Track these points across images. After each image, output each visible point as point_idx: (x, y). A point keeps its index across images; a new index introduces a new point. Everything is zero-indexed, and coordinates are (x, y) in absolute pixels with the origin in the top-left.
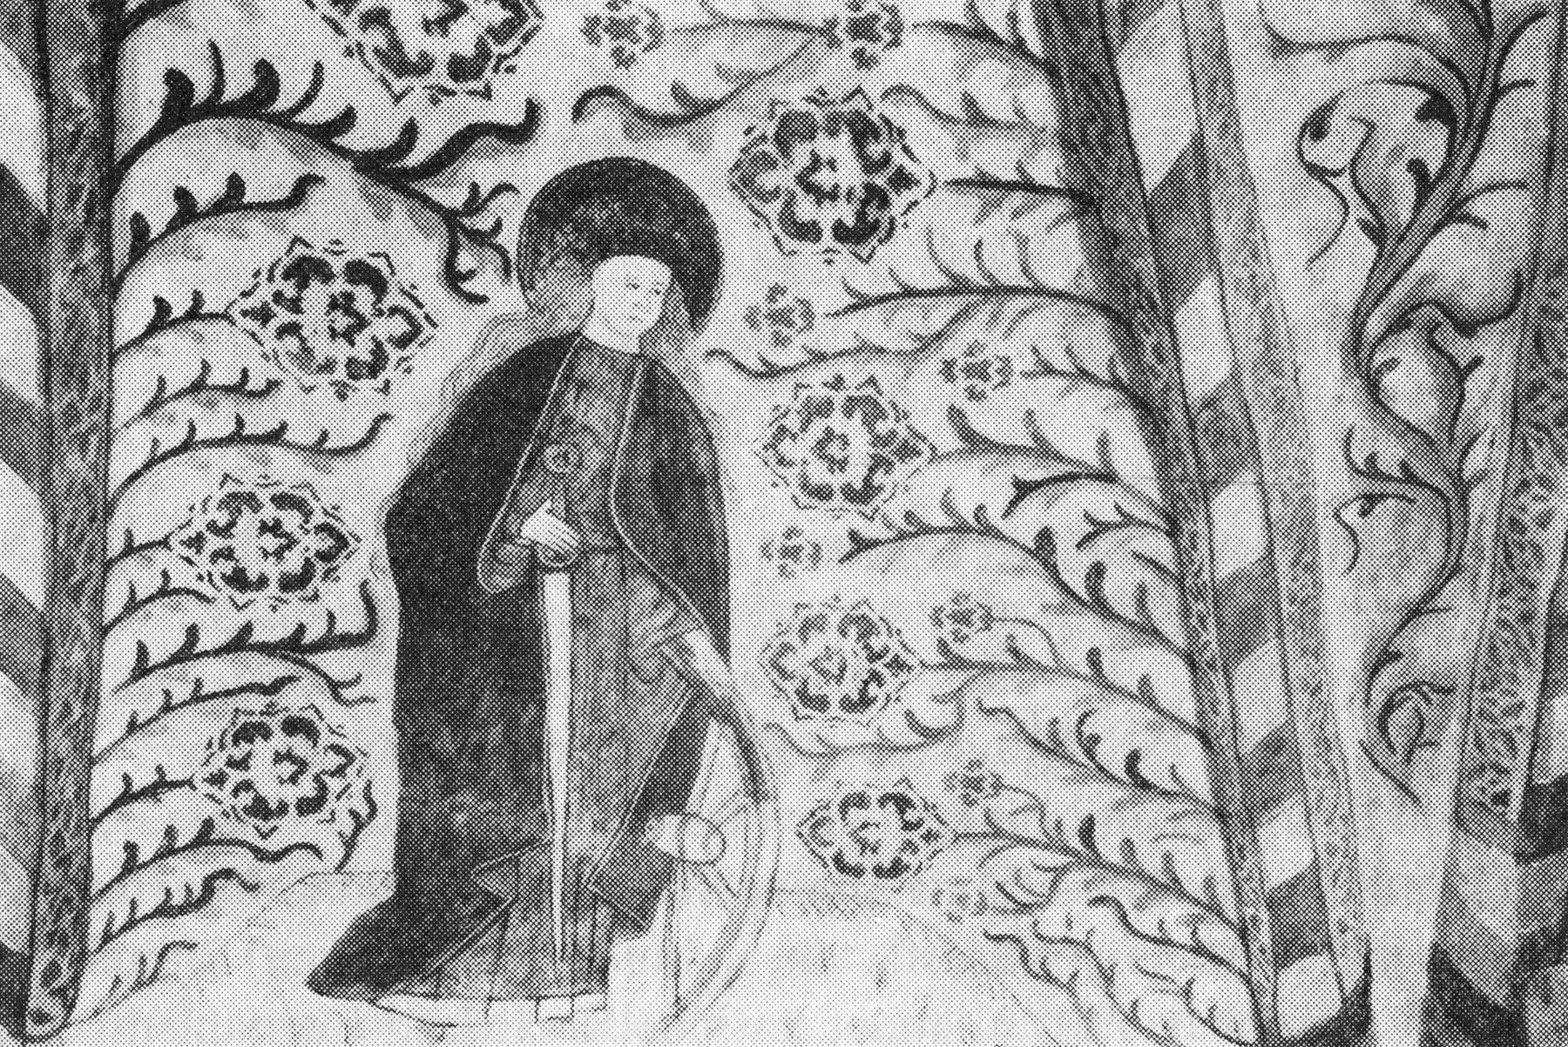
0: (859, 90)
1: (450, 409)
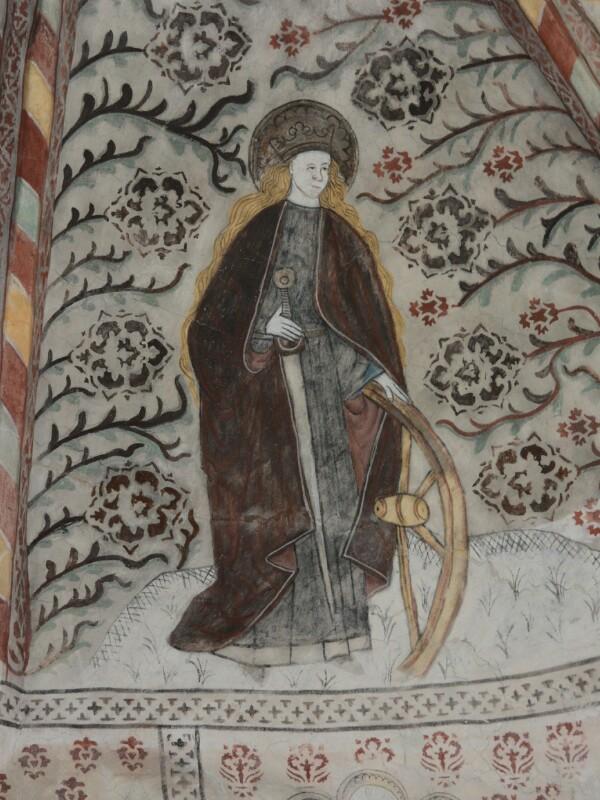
0: (406, 38)
1: (219, 259)
